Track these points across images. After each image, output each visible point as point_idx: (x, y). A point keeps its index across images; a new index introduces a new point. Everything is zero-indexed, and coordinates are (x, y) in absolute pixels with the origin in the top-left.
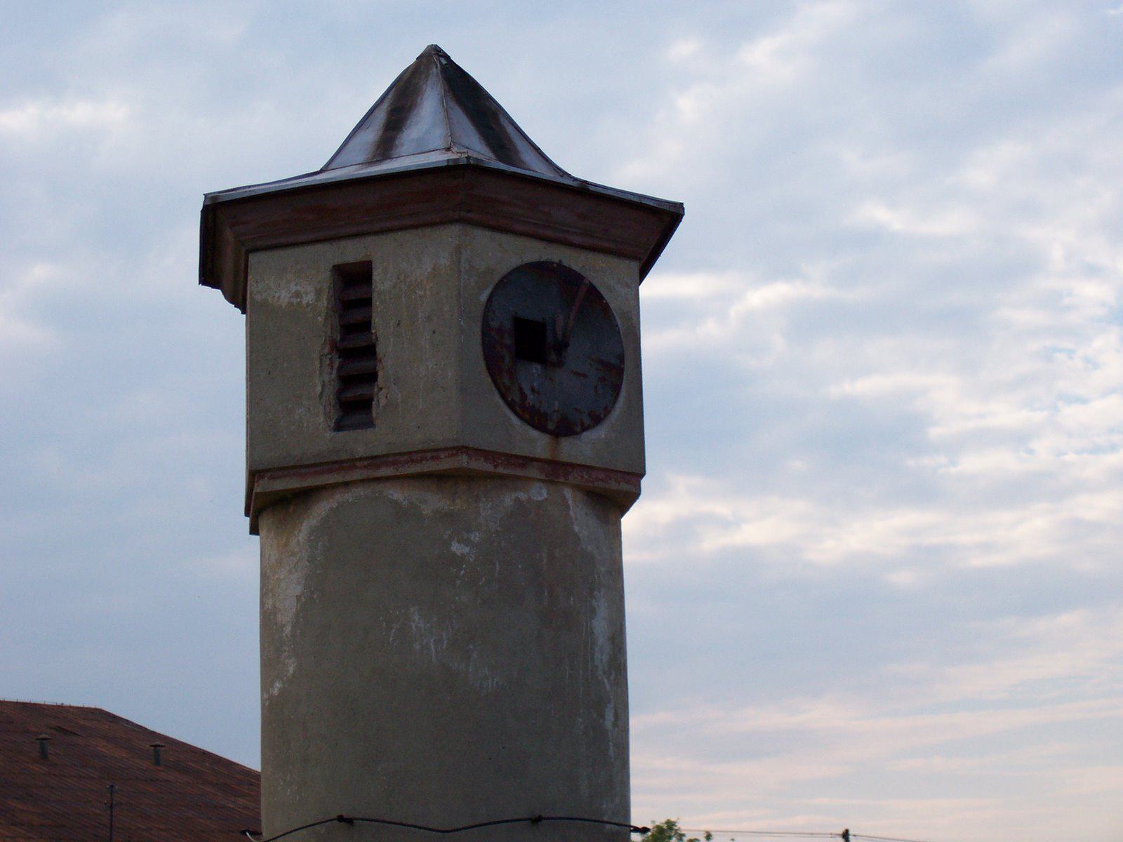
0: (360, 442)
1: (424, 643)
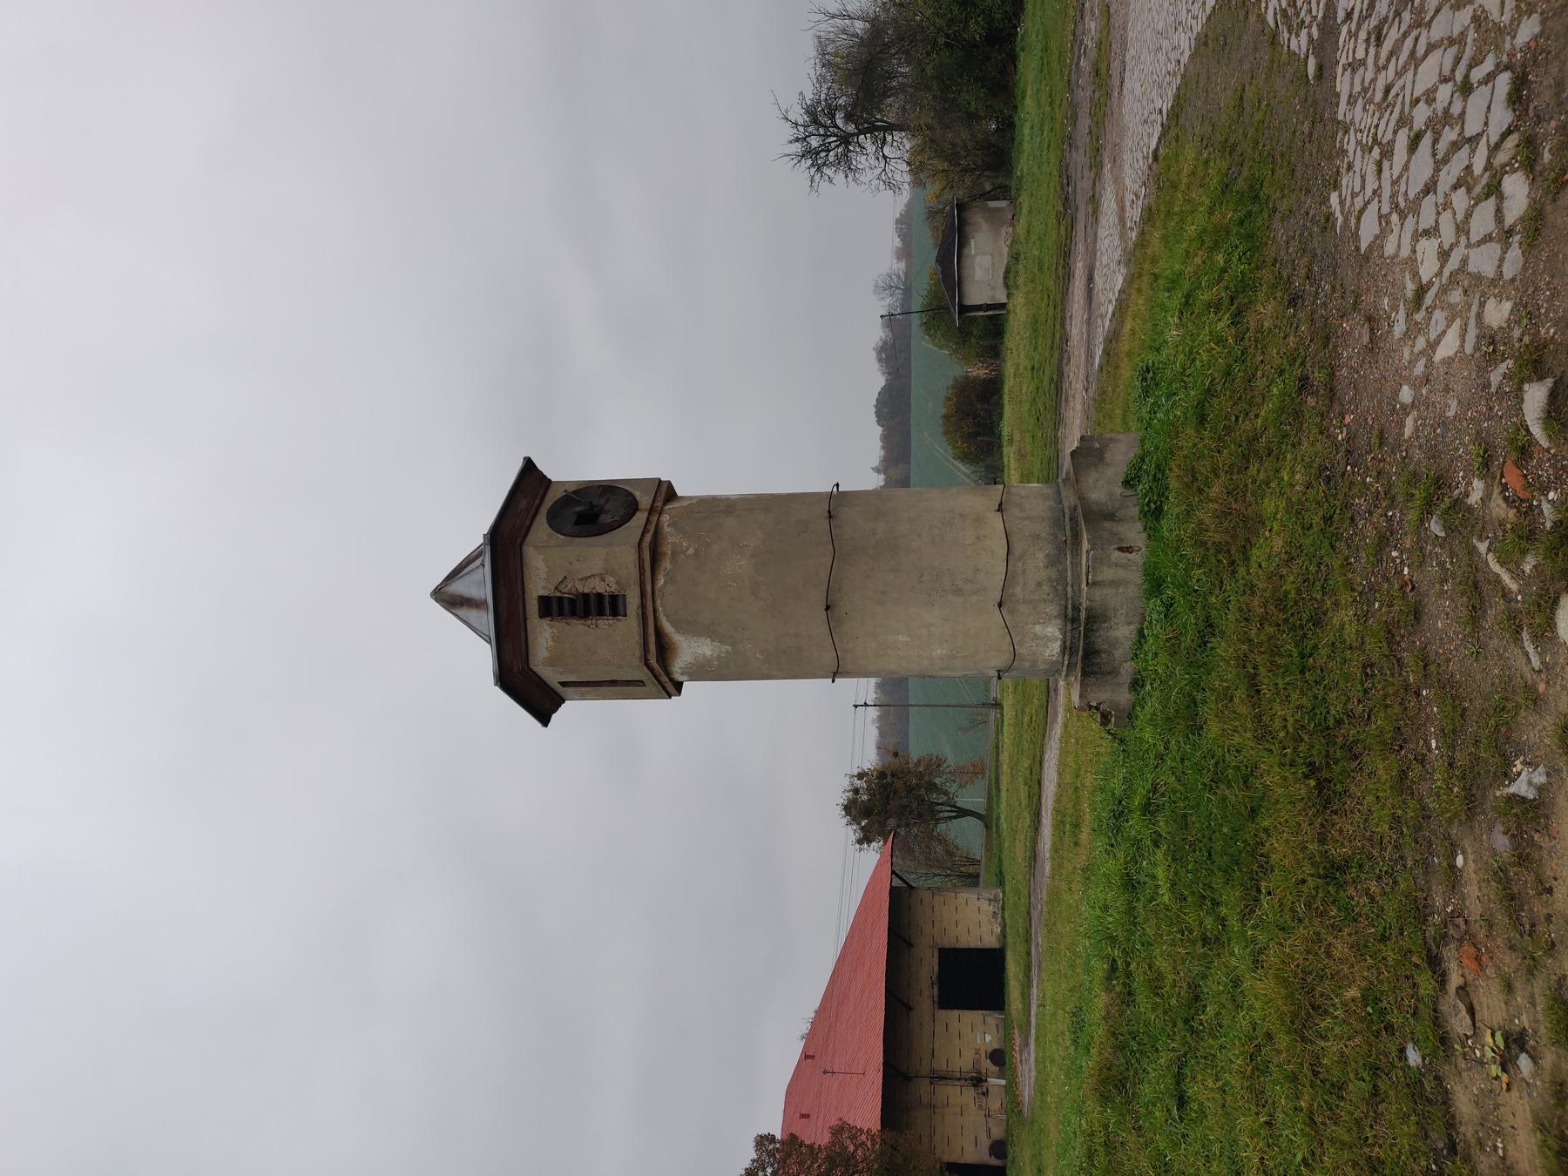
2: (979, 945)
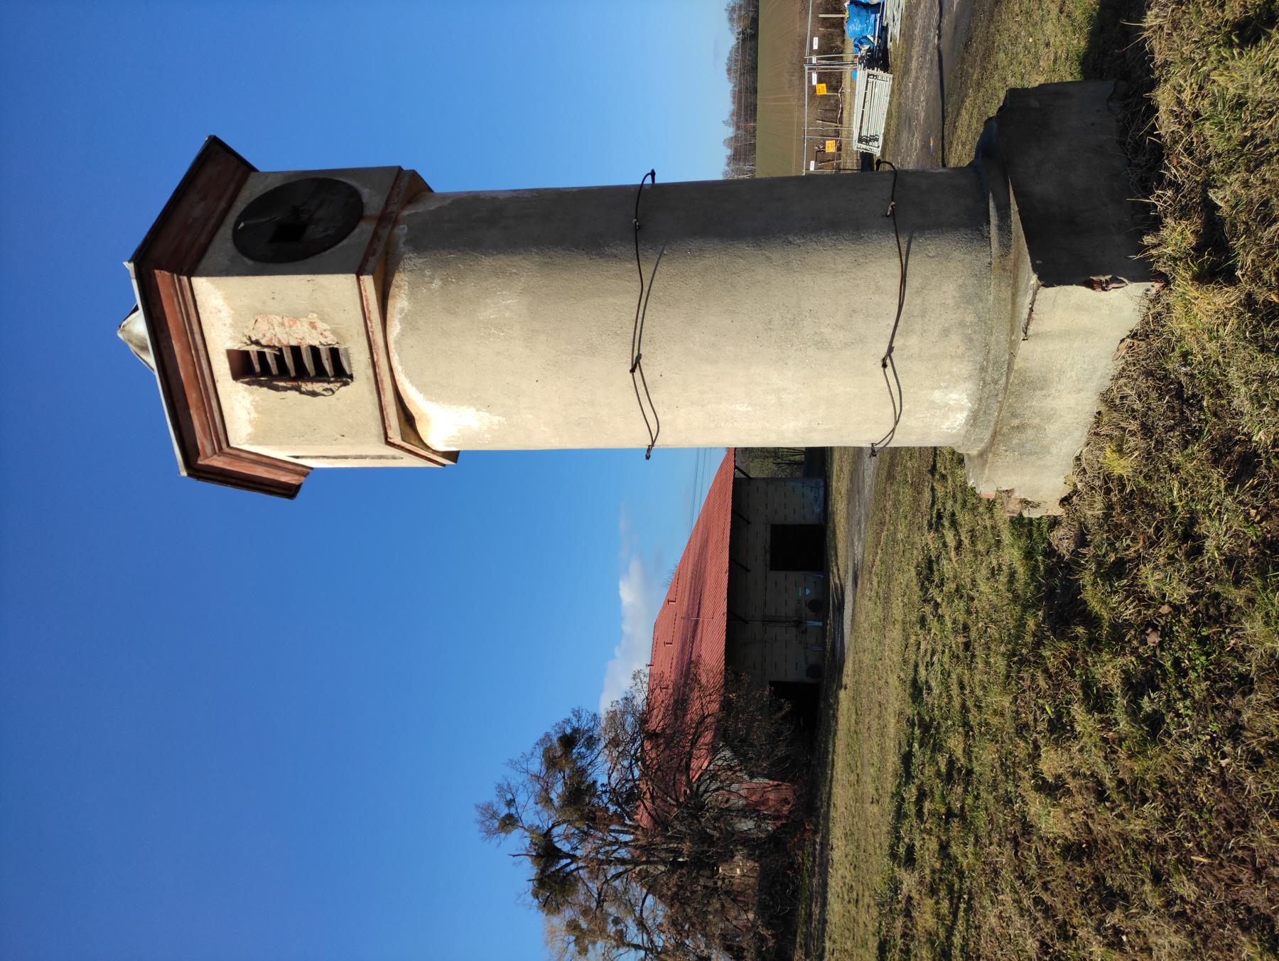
0: (357, 361)
1: (943, 769)
2: (803, 522)
